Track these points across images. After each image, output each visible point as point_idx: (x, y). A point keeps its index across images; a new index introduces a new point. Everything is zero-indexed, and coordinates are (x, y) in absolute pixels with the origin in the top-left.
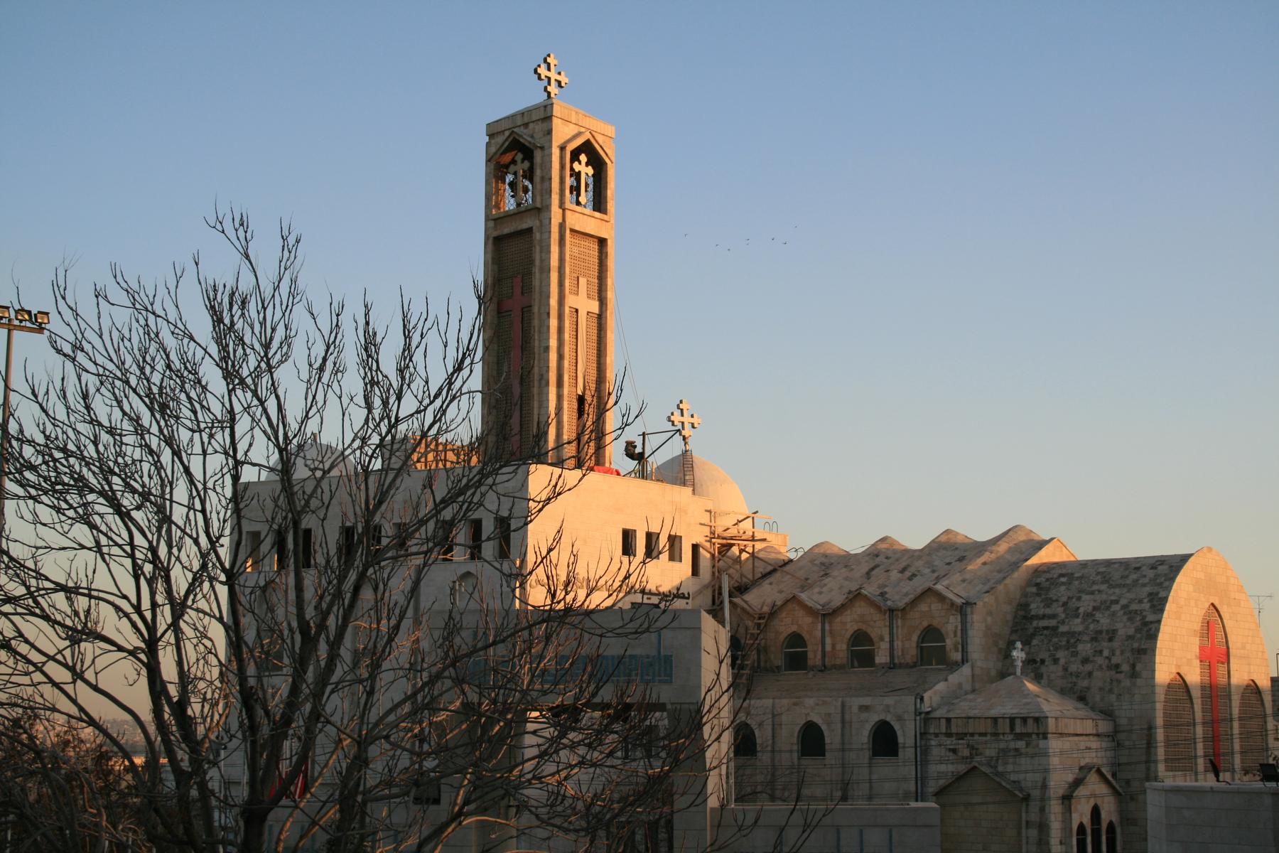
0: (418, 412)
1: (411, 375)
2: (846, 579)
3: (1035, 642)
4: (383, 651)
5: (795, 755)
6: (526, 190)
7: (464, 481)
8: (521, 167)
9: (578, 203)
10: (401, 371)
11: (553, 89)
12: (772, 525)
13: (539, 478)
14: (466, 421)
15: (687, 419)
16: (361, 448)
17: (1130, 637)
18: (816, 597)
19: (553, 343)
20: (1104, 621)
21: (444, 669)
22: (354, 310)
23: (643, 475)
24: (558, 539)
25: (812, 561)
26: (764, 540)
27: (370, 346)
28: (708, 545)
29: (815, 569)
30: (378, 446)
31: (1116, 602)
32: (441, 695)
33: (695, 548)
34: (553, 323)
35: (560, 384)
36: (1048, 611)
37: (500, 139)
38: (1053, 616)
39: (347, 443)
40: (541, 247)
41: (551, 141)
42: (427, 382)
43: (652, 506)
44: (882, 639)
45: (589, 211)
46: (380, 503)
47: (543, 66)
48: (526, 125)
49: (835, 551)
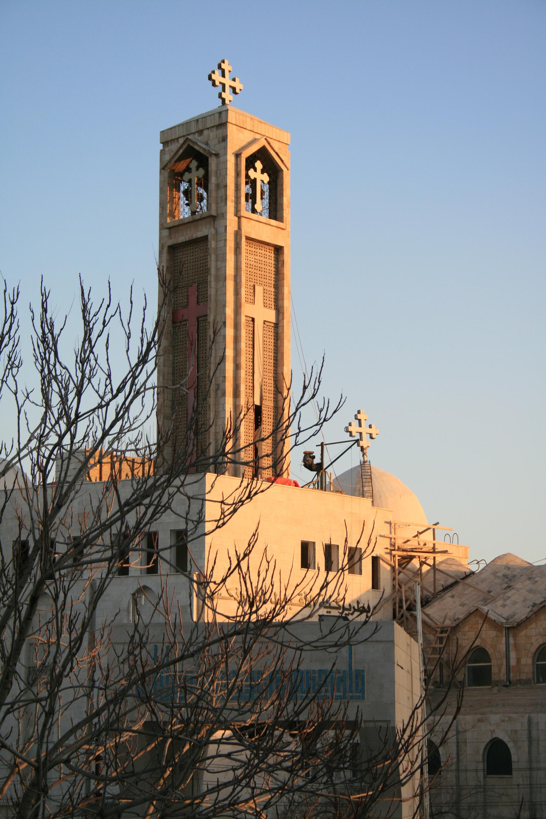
0: (100, 406)
1: (92, 370)
2: (530, 591)
4: (64, 667)
5: (481, 774)
6: (200, 198)
7: (150, 482)
8: (197, 174)
9: (254, 211)
10: (83, 361)
11: (228, 95)
12: (453, 537)
13: (221, 487)
14: (145, 425)
15: (365, 429)
16: (38, 448)
18: (500, 610)
19: (230, 353)
21: (130, 687)
22: (30, 299)
23: (321, 485)
24: (250, 546)
25: (495, 574)
26: (446, 552)
27: (48, 342)
28: (388, 557)
29: (497, 581)
30: (55, 446)
32: (125, 714)
33: (375, 560)
34: (230, 332)
35: (236, 394)
37: (174, 147)
39: (23, 443)
40: (217, 256)
41: (226, 148)
42: (109, 376)
43: (331, 518)
45: (264, 218)
46: (59, 506)
47: (218, 72)
48: (200, 132)
49: (518, 562)
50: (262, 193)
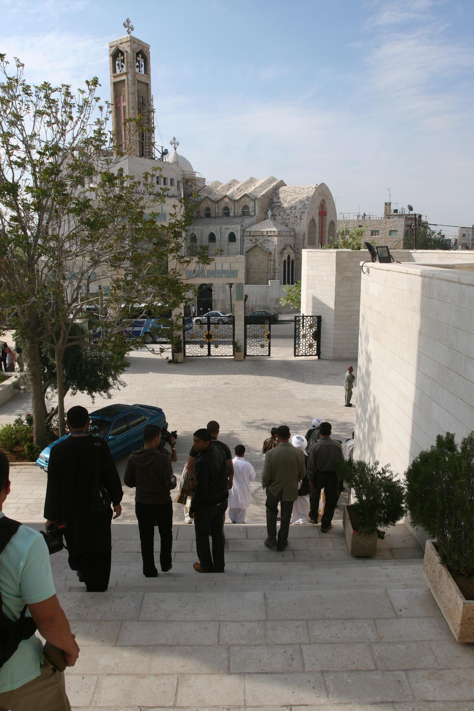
3: (274, 210)
17: (300, 208)
37: (114, 48)
44: (232, 209)
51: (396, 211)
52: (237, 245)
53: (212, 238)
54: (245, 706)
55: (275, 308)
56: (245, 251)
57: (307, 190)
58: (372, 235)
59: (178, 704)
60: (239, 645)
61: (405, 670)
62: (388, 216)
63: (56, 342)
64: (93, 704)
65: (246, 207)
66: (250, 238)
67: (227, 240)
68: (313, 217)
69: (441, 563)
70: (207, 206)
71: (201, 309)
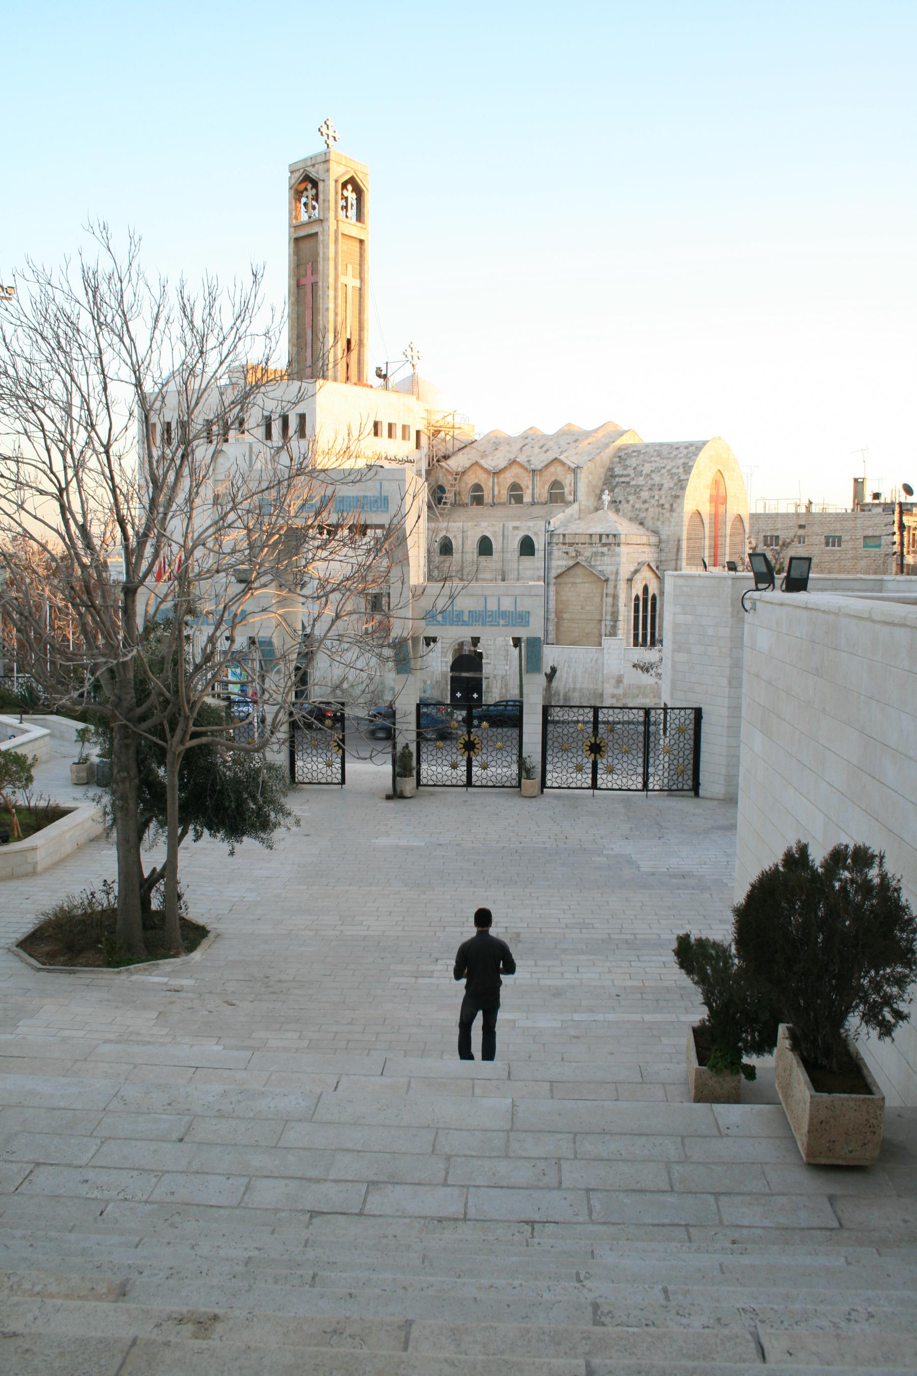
2: (508, 451)
3: (616, 490)
5: (475, 555)
6: (314, 208)
9: (347, 217)
11: (331, 141)
15: (415, 354)
17: (671, 489)
20: (657, 479)
25: (488, 441)
28: (426, 430)
31: (664, 468)
33: (418, 433)
34: (331, 293)
36: (625, 473)
37: (297, 175)
38: (628, 475)
44: (527, 487)
48: (313, 165)
50: (352, 205)
51: (876, 496)
52: (536, 563)
53: (485, 547)
54: (465, 1219)
55: (613, 696)
56: (554, 573)
57: (685, 451)
58: (827, 544)
59: (365, 1212)
60: (465, 1156)
61: (717, 1195)
62: (859, 504)
63: (168, 736)
64: (243, 1204)
65: (556, 484)
66: (565, 548)
67: (517, 554)
68: (697, 506)
69: (792, 1050)
70: (476, 481)
71: (459, 695)
